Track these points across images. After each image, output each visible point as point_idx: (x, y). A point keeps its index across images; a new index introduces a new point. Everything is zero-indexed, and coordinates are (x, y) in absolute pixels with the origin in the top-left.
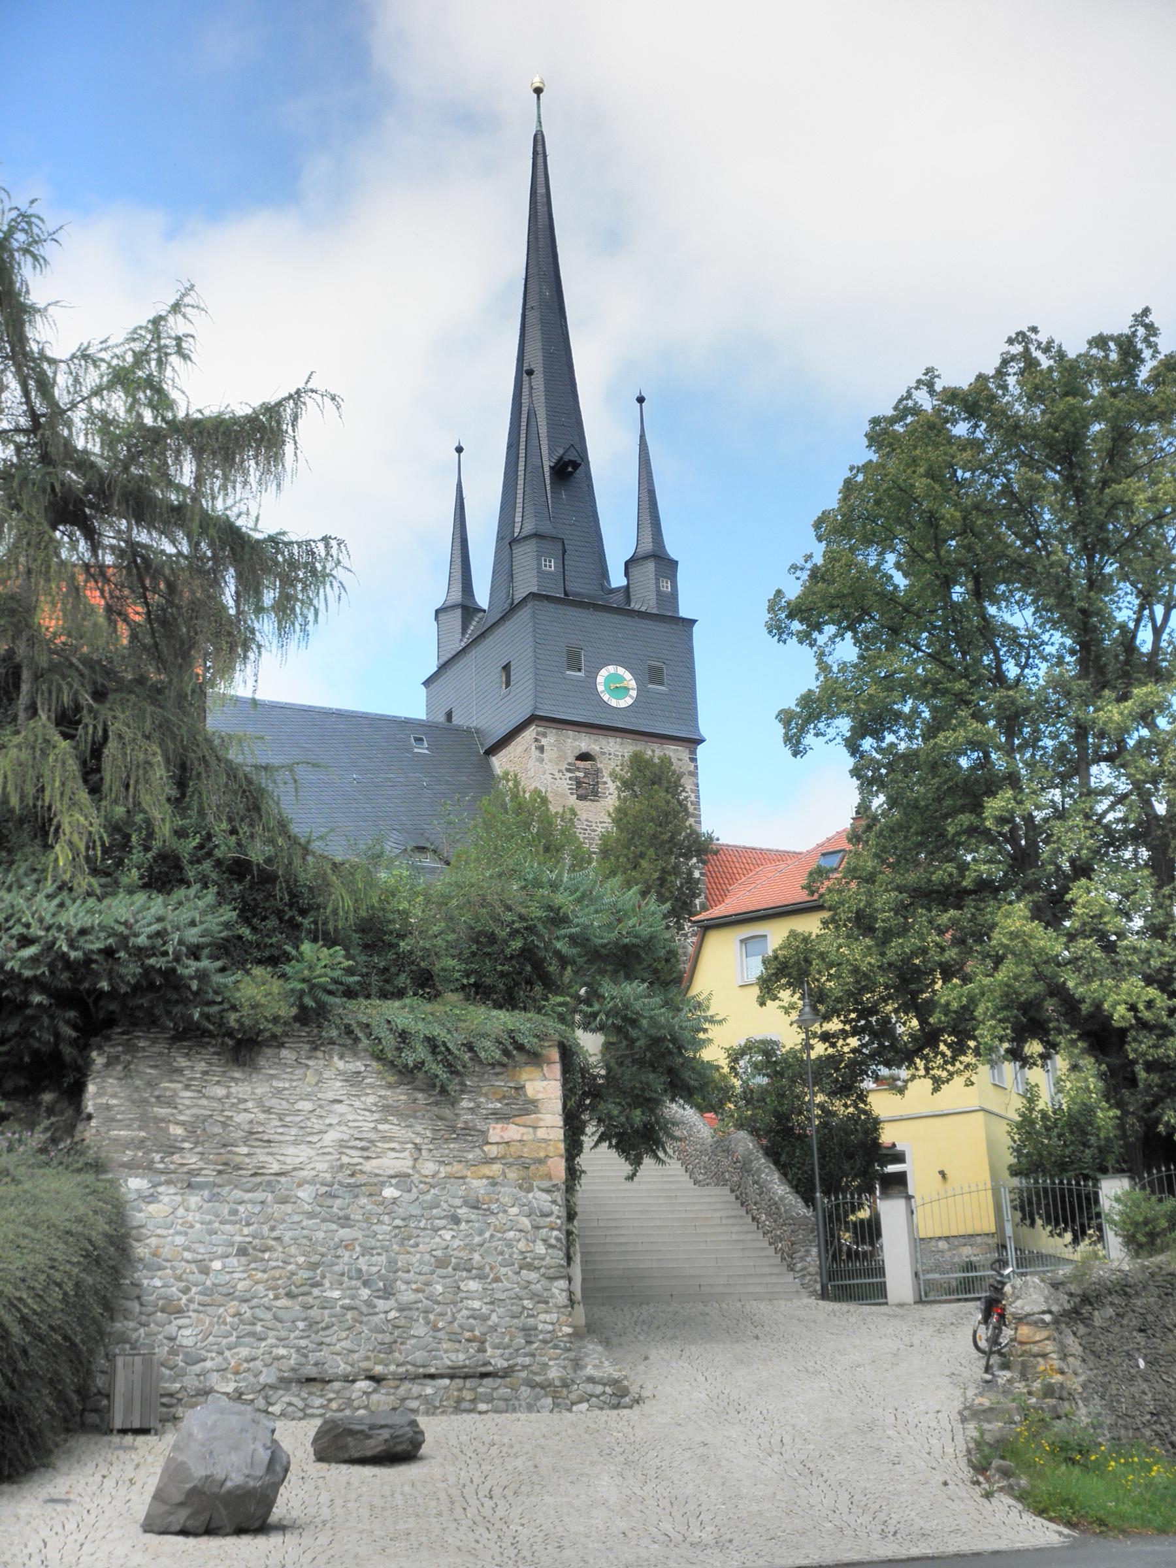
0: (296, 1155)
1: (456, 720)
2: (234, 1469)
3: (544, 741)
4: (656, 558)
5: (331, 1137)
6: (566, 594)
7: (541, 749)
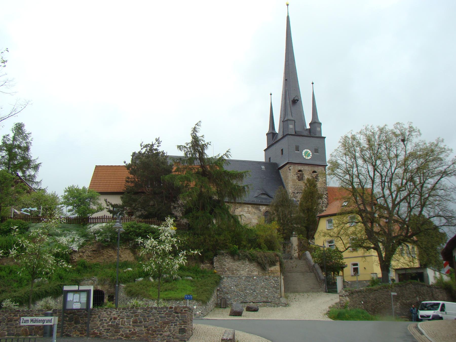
2: (238, 310)
3: (290, 168)
4: (315, 123)
5: (247, 270)
6: (295, 133)
7: (290, 170)
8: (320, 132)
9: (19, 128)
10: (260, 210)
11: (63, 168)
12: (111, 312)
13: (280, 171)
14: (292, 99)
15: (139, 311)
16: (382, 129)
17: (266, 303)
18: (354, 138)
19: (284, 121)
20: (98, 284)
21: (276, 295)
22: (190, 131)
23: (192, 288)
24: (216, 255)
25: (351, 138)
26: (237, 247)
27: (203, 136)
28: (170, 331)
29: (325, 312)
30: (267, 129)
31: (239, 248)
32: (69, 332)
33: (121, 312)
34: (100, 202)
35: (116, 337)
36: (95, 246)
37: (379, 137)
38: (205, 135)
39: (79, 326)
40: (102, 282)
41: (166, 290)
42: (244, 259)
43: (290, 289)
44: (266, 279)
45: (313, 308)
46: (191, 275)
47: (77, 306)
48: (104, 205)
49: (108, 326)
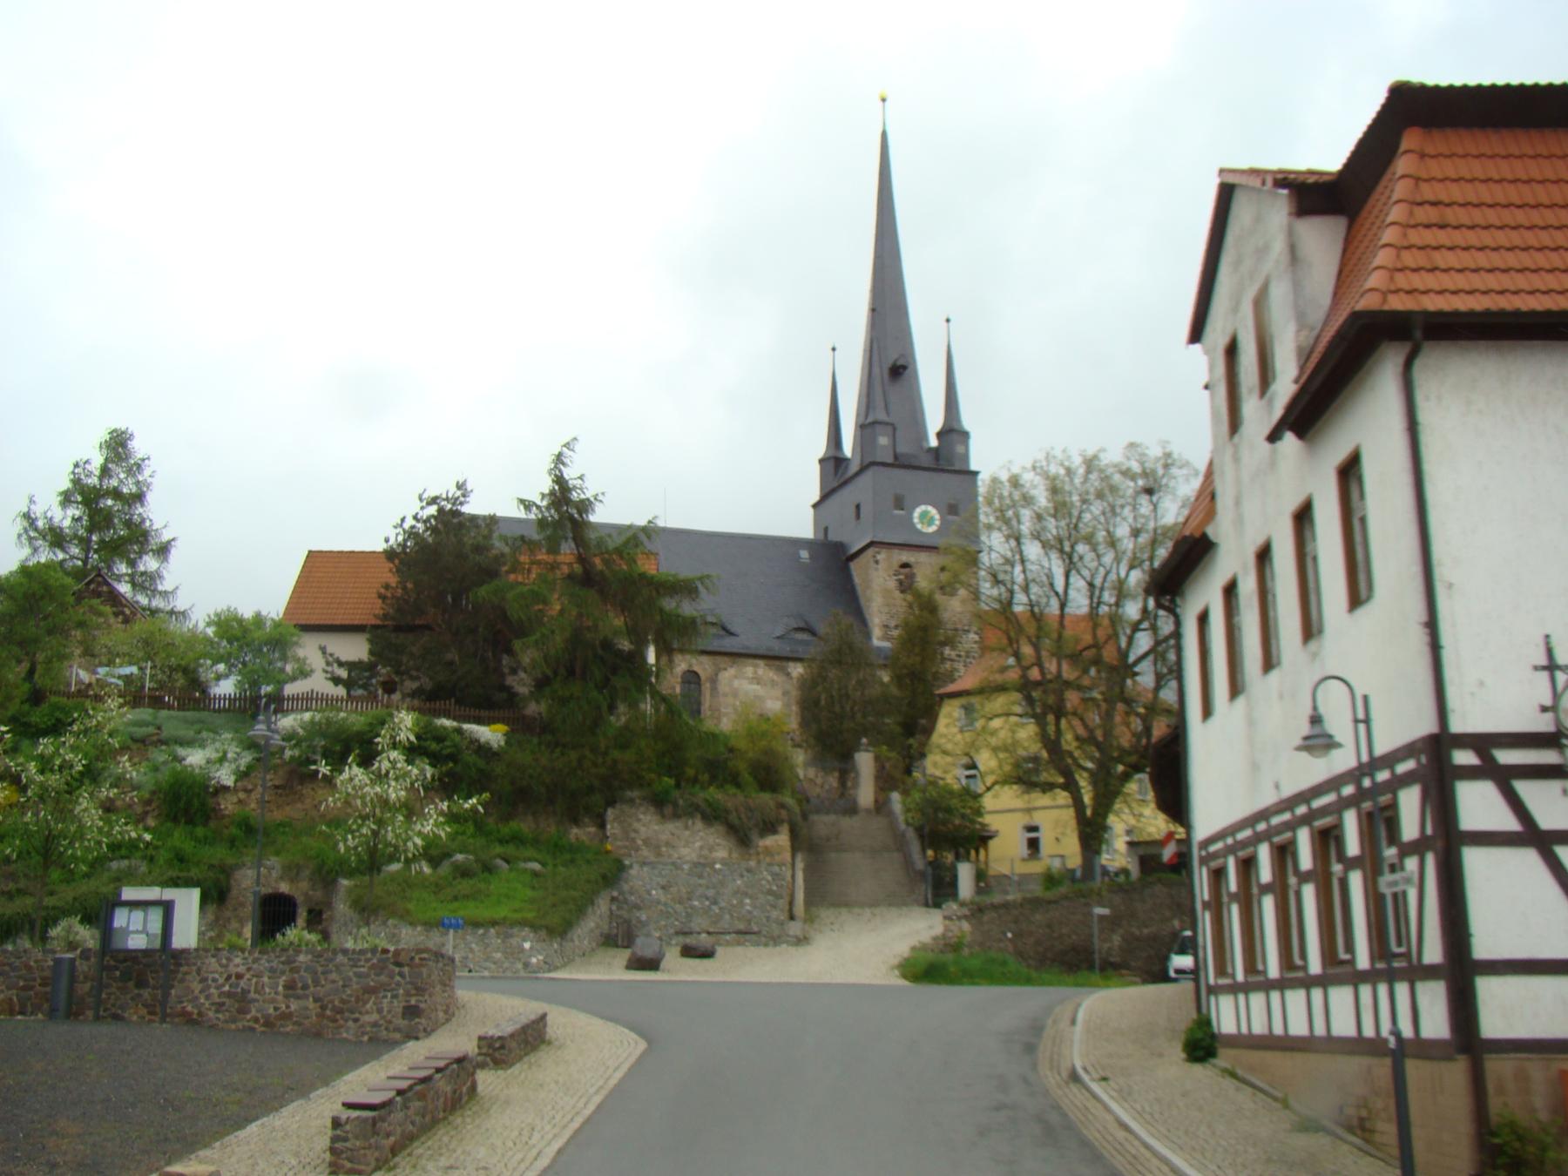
0: (685, 851)
4: (953, 432)
7: (877, 562)
8: (966, 457)
9: (118, 445)
10: (788, 674)
11: (226, 559)
12: (229, 959)
13: (853, 565)
14: (890, 363)
15: (302, 958)
16: (1095, 457)
17: (746, 934)
18: (1015, 482)
19: (865, 428)
20: (281, 878)
21: (774, 914)
22: (548, 463)
23: (530, 893)
24: (611, 803)
25: (1010, 481)
26: (672, 782)
27: (581, 478)
28: (380, 1011)
29: (896, 961)
30: (820, 447)
31: (678, 785)
32: (121, 1007)
33: (256, 961)
34: (301, 653)
35: (240, 1025)
36: (281, 773)
37: (1086, 480)
38: (589, 477)
39: (146, 994)
40: (291, 872)
41: (456, 898)
42: (691, 815)
43: (825, 895)
44: (749, 870)
45: (867, 949)
46: (539, 857)
47: (137, 942)
48: (316, 661)
49: (221, 994)
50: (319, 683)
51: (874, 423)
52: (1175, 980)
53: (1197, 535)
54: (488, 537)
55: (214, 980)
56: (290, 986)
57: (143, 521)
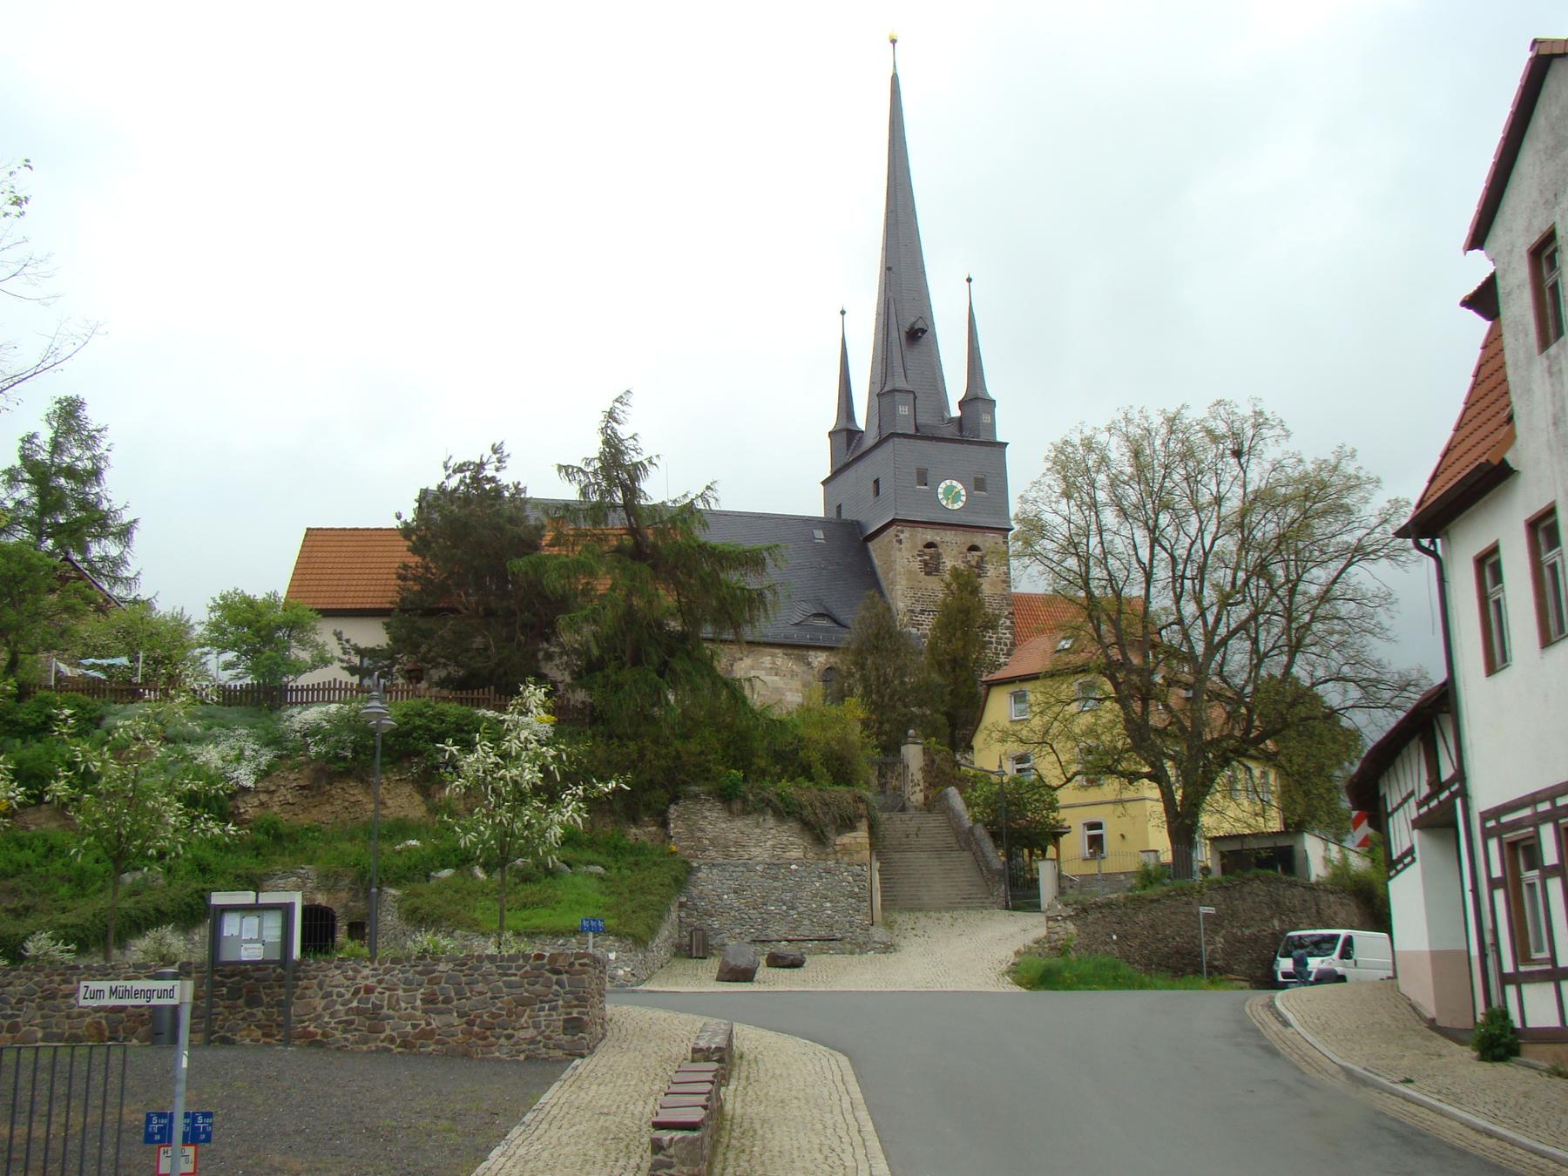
0: (755, 851)
1: (844, 516)
2: (742, 962)
4: (977, 400)
5: (769, 843)
6: (917, 429)
7: (900, 542)
8: (992, 427)
9: (69, 414)
10: (809, 664)
11: (205, 534)
12: (356, 971)
14: (907, 327)
15: (442, 967)
17: (828, 941)
18: (1089, 445)
19: (883, 395)
20: (318, 889)
21: (858, 918)
22: (598, 420)
23: (603, 899)
24: (674, 799)
26: (741, 774)
28: (536, 1026)
30: (830, 420)
33: (387, 972)
34: (320, 639)
35: (373, 1046)
36: (307, 772)
38: (645, 434)
39: (259, 1012)
41: (525, 906)
42: (762, 812)
43: (901, 899)
47: (251, 953)
50: (335, 673)
51: (894, 391)
52: (1283, 986)
53: (1495, 462)
54: (520, 509)
55: (340, 995)
56: (429, 1000)
57: (100, 501)
